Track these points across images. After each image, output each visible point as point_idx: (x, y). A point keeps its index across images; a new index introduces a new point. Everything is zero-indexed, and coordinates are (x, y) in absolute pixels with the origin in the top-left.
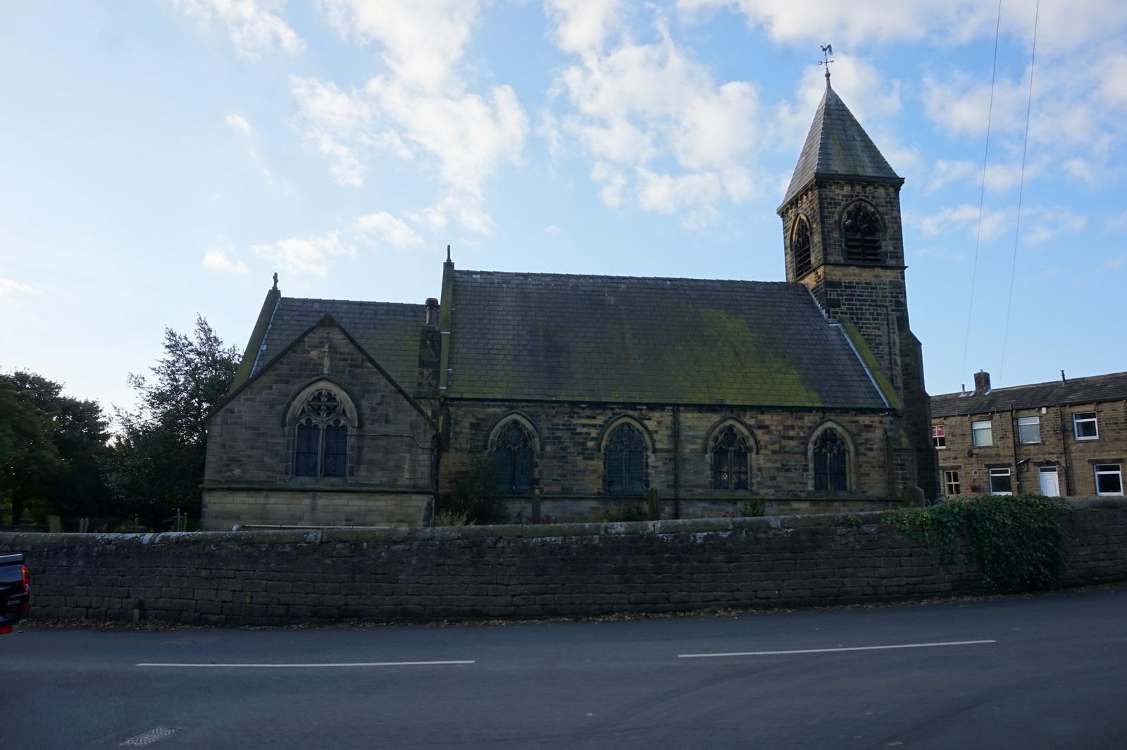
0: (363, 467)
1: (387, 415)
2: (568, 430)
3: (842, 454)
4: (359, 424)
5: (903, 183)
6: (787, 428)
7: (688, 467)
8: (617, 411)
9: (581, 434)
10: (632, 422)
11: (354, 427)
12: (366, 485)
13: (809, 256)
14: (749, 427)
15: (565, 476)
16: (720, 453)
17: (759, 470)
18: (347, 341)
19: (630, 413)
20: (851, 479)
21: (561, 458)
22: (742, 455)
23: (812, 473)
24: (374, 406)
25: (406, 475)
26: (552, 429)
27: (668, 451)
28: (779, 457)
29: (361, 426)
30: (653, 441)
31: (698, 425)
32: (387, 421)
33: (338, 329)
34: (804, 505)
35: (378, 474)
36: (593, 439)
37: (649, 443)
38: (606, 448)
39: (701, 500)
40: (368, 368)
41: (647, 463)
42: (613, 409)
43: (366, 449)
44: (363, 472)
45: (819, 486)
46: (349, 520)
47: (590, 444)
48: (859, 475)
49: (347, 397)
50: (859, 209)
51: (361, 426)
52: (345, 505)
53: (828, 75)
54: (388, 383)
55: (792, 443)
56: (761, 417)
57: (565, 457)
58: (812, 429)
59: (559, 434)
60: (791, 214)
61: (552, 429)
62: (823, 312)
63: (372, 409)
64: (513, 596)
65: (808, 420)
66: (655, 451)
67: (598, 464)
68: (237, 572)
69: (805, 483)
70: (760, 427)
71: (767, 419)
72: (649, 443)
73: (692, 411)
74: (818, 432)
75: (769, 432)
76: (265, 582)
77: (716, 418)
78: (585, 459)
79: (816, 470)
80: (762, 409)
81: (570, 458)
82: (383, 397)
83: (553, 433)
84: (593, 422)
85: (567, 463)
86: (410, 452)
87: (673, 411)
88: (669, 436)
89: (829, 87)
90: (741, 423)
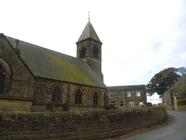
0: (11, 91)
1: (21, 74)
2: (44, 86)
3: (98, 96)
4: (11, 75)
5: (99, 43)
6: (89, 90)
7: (70, 98)
8: (56, 82)
9: (47, 87)
10: (60, 85)
11: (9, 76)
12: (12, 97)
13: (85, 54)
14: (83, 90)
15: (42, 99)
16: (77, 95)
17: (84, 99)
18: (9, 45)
19: (59, 83)
20: (99, 102)
21: (42, 93)
22: (81, 96)
23: (93, 101)
24: (17, 69)
25: (26, 94)
26: (40, 85)
27: (67, 94)
28: (87, 97)
29: (11, 76)
30: (64, 91)
31: (73, 88)
32: (21, 75)
33: (5, 40)
34: (91, 108)
35: (17, 93)
36: (50, 89)
37: (63, 91)
38: (53, 92)
39: (73, 106)
40: (16, 56)
41: (62, 96)
42: (56, 82)
43: (13, 84)
44: (11, 92)
45: (94, 104)
46: (4, 110)
47: (49, 90)
48: (100, 101)
49: (7, 64)
50: (95, 47)
51: (11, 76)
52: (3, 104)
53: (89, 18)
54: (22, 62)
55: (90, 94)
56: (85, 87)
57: (43, 93)
58: (93, 91)
59: (42, 87)
60: (80, 44)
61: (40, 85)
62: (88, 66)
63: (16, 71)
64: (107, 131)
65: (93, 89)
66: (64, 93)
67: (51, 96)
68: (12, 132)
69: (92, 103)
70: (84, 90)
71: (86, 88)
72: (63, 91)
73: (72, 85)
74: (94, 92)
75: (86, 91)
76: (27, 135)
77: (77, 87)
78: (48, 94)
79: (93, 100)
80: (85, 86)
81: (44, 94)
82: (20, 67)
83: (40, 86)
84: (50, 84)
85: (43, 95)
86: (28, 87)
87: (69, 84)
88: (67, 90)
89: (89, 21)
90: (81, 88)
